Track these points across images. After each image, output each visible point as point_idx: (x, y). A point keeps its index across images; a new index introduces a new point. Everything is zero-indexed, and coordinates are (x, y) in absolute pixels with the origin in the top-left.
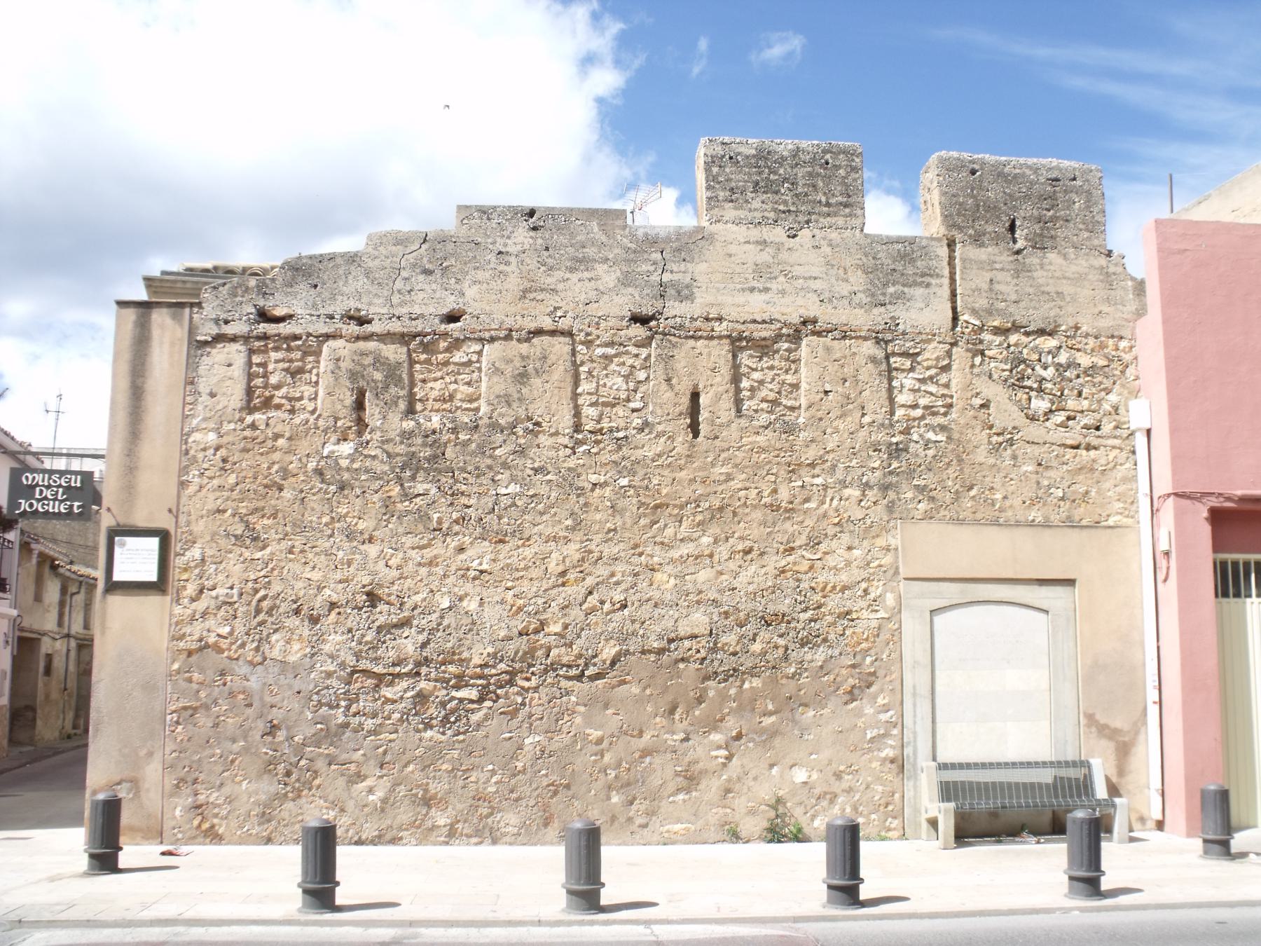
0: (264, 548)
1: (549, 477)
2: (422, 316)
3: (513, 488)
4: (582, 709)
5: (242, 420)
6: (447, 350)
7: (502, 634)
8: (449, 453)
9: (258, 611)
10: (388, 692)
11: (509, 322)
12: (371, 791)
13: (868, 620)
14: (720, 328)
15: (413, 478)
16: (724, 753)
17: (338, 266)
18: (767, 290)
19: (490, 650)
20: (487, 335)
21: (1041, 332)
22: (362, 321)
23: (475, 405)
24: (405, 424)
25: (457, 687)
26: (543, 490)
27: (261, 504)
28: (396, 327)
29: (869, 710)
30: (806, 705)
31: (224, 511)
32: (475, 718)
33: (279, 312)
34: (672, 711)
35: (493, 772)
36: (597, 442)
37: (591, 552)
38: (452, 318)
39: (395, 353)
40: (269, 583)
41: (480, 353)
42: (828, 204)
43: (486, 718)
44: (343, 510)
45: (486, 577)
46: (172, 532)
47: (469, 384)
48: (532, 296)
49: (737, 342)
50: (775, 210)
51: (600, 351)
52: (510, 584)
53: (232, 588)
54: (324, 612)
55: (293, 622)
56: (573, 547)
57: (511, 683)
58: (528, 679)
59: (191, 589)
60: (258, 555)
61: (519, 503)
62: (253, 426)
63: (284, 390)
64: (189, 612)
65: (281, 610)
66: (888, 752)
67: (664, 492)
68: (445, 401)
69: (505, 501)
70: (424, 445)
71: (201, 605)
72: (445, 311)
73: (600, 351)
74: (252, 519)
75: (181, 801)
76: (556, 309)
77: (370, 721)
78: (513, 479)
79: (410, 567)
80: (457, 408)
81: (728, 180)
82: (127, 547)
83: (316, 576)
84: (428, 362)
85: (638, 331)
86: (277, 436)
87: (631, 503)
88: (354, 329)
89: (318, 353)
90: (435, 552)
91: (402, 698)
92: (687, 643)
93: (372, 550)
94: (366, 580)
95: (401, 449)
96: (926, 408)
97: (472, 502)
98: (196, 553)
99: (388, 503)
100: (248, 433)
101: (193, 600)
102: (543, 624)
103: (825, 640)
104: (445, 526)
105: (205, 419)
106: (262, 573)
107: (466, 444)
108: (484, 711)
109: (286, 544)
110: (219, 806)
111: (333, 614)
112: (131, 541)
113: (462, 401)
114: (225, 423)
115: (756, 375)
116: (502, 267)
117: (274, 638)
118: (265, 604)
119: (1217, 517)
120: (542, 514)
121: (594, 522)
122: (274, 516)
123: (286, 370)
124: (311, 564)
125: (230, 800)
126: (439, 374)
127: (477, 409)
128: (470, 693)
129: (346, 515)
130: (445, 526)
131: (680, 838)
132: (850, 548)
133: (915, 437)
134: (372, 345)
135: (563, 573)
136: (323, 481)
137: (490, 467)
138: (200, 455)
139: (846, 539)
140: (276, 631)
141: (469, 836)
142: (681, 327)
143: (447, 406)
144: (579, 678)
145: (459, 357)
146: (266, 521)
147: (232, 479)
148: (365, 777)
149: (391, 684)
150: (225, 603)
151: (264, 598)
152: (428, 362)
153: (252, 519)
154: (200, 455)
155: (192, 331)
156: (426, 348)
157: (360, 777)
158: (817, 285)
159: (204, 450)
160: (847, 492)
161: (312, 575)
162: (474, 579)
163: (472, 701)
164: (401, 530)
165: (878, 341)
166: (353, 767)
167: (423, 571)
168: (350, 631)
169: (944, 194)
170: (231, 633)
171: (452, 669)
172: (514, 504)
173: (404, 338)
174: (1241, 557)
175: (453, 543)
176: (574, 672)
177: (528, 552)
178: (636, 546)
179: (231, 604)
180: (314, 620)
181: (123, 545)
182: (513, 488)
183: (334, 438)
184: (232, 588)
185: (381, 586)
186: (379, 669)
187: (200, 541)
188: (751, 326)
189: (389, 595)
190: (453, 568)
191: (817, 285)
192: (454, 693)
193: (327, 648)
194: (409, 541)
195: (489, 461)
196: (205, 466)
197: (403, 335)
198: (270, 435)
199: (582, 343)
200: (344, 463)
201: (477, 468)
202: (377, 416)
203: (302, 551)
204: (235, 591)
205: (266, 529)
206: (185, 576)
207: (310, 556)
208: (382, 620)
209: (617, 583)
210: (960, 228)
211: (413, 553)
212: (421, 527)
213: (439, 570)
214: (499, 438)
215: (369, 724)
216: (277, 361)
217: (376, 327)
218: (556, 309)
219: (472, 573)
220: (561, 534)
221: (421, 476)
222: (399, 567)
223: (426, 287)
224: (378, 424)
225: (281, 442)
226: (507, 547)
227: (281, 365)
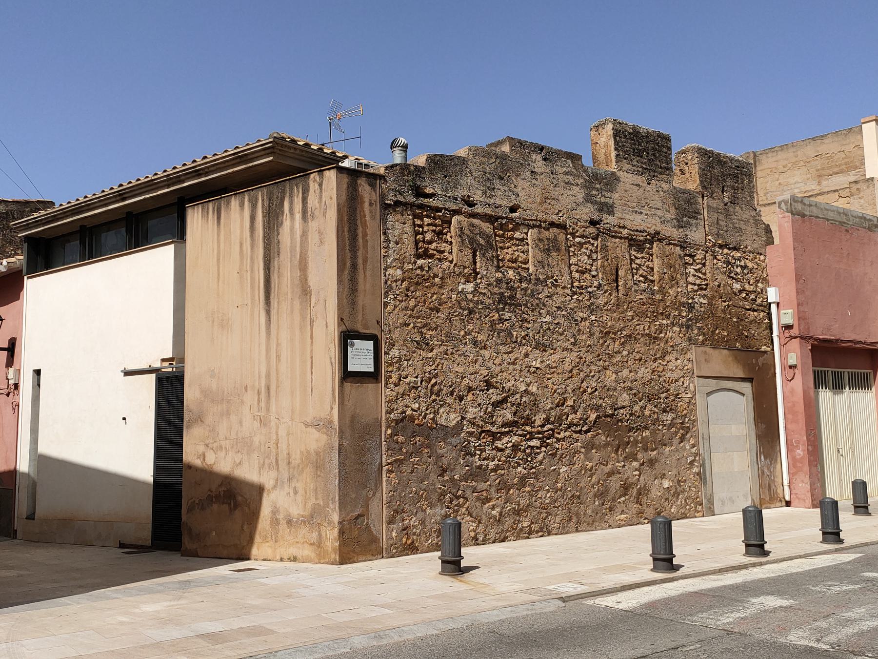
0: (431, 351)
1: (563, 313)
2: (500, 206)
3: (548, 319)
4: (583, 450)
5: (415, 263)
6: (512, 230)
7: (549, 406)
8: (518, 296)
9: (432, 393)
10: (499, 444)
11: (541, 216)
12: (493, 508)
13: (686, 397)
14: (625, 232)
15: (503, 310)
16: (637, 473)
17: (456, 165)
18: (641, 213)
19: (544, 416)
20: (531, 223)
21: (735, 249)
22: (471, 204)
23: (527, 266)
24: (497, 275)
25: (530, 440)
26: (561, 320)
27: (428, 321)
28: (489, 211)
29: (688, 447)
30: (665, 445)
31: (409, 324)
32: (540, 457)
33: (429, 190)
34: (617, 451)
35: (548, 491)
36: (581, 293)
37: (581, 358)
38: (513, 209)
39: (487, 227)
40: (437, 374)
41: (527, 234)
42: (661, 168)
43: (544, 458)
44: (470, 327)
45: (539, 372)
46: (379, 337)
47: (523, 252)
48: (549, 201)
49: (633, 242)
50: (642, 167)
51: (577, 240)
52: (549, 376)
53: (417, 377)
54: (465, 393)
55: (450, 400)
56: (575, 354)
57: (553, 436)
58: (559, 433)
59: (394, 378)
60: (430, 355)
61: (551, 328)
62: (421, 268)
63: (434, 246)
64: (395, 394)
65: (444, 392)
66: (695, 470)
67: (609, 324)
68: (513, 262)
69: (545, 326)
70: (507, 288)
71: (400, 389)
72: (511, 205)
73: (577, 240)
74: (424, 330)
75: (395, 526)
76: (560, 211)
77: (492, 464)
78: (548, 313)
79: (505, 365)
80: (519, 267)
81: (623, 146)
82: (355, 347)
83: (460, 369)
84: (503, 236)
85: (592, 230)
86: (436, 276)
87: (596, 330)
88: (466, 208)
89: (450, 223)
90: (516, 356)
91: (506, 447)
92: (622, 411)
93: (486, 353)
94: (485, 373)
95: (496, 290)
96: (699, 285)
97: (530, 326)
98: (395, 352)
99: (493, 324)
100: (418, 272)
101: (396, 385)
102: (565, 399)
103: (671, 409)
104: (519, 339)
105: (395, 260)
106: (433, 367)
107: (526, 289)
108: (543, 454)
109: (443, 348)
110: (414, 527)
111: (470, 395)
112: (358, 343)
113: (521, 262)
114: (406, 264)
115: (638, 261)
116: (534, 181)
117: (442, 410)
118: (436, 388)
119: (814, 349)
120: (561, 335)
121: (582, 340)
122: (436, 329)
123: (434, 231)
124: (457, 362)
125: (423, 522)
126: (508, 244)
127: (528, 269)
128: (535, 443)
129: (472, 331)
130: (519, 339)
131: (623, 523)
132: (677, 359)
133: (696, 300)
134: (476, 222)
135: (571, 371)
136: (461, 308)
137: (537, 305)
138: (394, 285)
139: (675, 354)
140: (442, 406)
141: (537, 532)
142: (609, 230)
143: (514, 265)
144: (580, 432)
145: (517, 235)
146: (431, 333)
147: (412, 303)
148: (491, 499)
149: (500, 439)
150: (414, 387)
151: (435, 384)
152: (503, 236)
153: (424, 330)
154: (394, 285)
155: (383, 197)
156: (502, 227)
157: (488, 500)
158: (659, 213)
159: (396, 281)
160: (675, 328)
161: (461, 369)
162: (534, 373)
163: (538, 448)
164: (499, 341)
165: (681, 247)
166: (484, 493)
167: (511, 367)
168: (479, 405)
169: (700, 168)
170: (419, 408)
171: (528, 428)
172: (549, 329)
173: (490, 219)
174: (856, 371)
175: (523, 350)
176: (578, 429)
177: (556, 357)
178: (599, 355)
179: (417, 388)
180: (461, 399)
181: (353, 345)
182: (548, 319)
183: (463, 280)
184: (417, 377)
185: (492, 377)
186: (494, 429)
187: (397, 344)
188: (637, 233)
189: (497, 382)
190: (524, 366)
191: (659, 213)
192: (529, 443)
193: (469, 416)
194: (503, 348)
195: (537, 301)
196: (397, 292)
197: (491, 216)
198: (460, 289)
199: (570, 234)
200: (470, 297)
201: (532, 305)
202: (484, 268)
203: (452, 354)
204: (419, 379)
205: (432, 337)
206: (390, 369)
207: (456, 356)
208: (494, 398)
209: (593, 377)
210: (706, 188)
211: (505, 356)
212: (508, 340)
213: (517, 367)
214: (540, 287)
215: (492, 464)
216: (428, 225)
217: (479, 209)
218: (560, 211)
219: (533, 369)
220: (570, 347)
221: (507, 308)
222: (500, 365)
223: (501, 187)
224: (485, 273)
225: (437, 280)
226: (547, 354)
227: (432, 228)
